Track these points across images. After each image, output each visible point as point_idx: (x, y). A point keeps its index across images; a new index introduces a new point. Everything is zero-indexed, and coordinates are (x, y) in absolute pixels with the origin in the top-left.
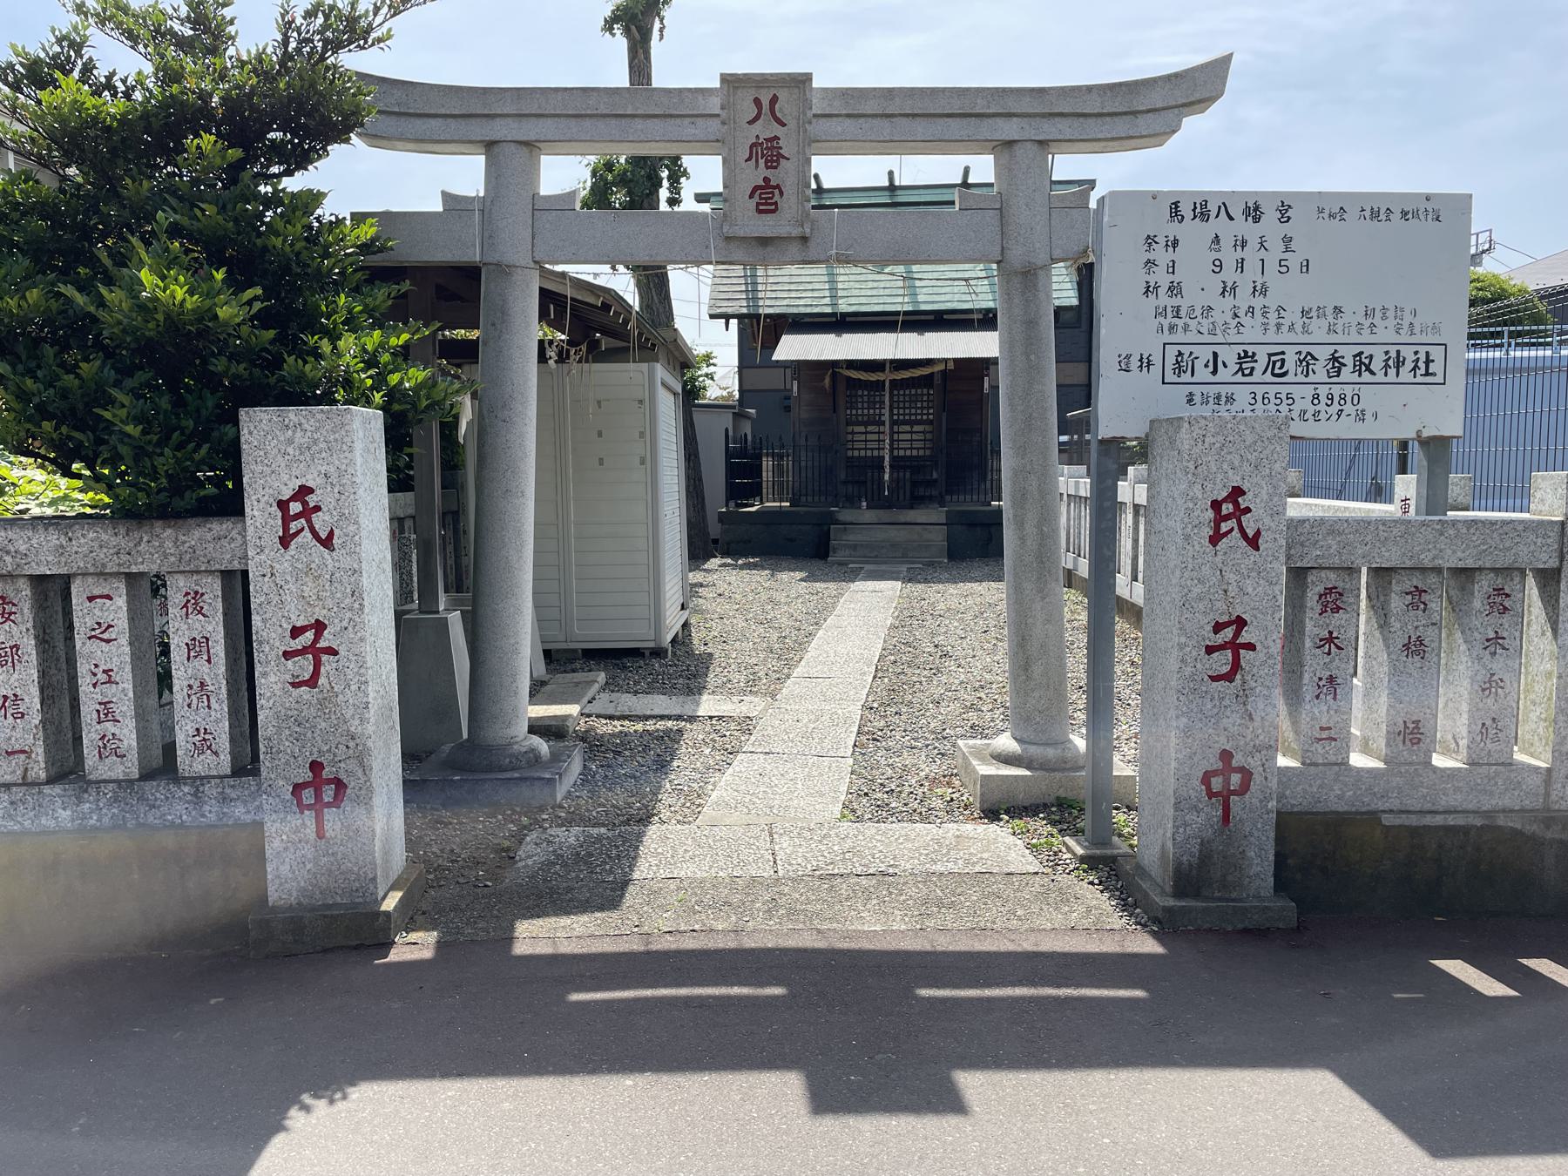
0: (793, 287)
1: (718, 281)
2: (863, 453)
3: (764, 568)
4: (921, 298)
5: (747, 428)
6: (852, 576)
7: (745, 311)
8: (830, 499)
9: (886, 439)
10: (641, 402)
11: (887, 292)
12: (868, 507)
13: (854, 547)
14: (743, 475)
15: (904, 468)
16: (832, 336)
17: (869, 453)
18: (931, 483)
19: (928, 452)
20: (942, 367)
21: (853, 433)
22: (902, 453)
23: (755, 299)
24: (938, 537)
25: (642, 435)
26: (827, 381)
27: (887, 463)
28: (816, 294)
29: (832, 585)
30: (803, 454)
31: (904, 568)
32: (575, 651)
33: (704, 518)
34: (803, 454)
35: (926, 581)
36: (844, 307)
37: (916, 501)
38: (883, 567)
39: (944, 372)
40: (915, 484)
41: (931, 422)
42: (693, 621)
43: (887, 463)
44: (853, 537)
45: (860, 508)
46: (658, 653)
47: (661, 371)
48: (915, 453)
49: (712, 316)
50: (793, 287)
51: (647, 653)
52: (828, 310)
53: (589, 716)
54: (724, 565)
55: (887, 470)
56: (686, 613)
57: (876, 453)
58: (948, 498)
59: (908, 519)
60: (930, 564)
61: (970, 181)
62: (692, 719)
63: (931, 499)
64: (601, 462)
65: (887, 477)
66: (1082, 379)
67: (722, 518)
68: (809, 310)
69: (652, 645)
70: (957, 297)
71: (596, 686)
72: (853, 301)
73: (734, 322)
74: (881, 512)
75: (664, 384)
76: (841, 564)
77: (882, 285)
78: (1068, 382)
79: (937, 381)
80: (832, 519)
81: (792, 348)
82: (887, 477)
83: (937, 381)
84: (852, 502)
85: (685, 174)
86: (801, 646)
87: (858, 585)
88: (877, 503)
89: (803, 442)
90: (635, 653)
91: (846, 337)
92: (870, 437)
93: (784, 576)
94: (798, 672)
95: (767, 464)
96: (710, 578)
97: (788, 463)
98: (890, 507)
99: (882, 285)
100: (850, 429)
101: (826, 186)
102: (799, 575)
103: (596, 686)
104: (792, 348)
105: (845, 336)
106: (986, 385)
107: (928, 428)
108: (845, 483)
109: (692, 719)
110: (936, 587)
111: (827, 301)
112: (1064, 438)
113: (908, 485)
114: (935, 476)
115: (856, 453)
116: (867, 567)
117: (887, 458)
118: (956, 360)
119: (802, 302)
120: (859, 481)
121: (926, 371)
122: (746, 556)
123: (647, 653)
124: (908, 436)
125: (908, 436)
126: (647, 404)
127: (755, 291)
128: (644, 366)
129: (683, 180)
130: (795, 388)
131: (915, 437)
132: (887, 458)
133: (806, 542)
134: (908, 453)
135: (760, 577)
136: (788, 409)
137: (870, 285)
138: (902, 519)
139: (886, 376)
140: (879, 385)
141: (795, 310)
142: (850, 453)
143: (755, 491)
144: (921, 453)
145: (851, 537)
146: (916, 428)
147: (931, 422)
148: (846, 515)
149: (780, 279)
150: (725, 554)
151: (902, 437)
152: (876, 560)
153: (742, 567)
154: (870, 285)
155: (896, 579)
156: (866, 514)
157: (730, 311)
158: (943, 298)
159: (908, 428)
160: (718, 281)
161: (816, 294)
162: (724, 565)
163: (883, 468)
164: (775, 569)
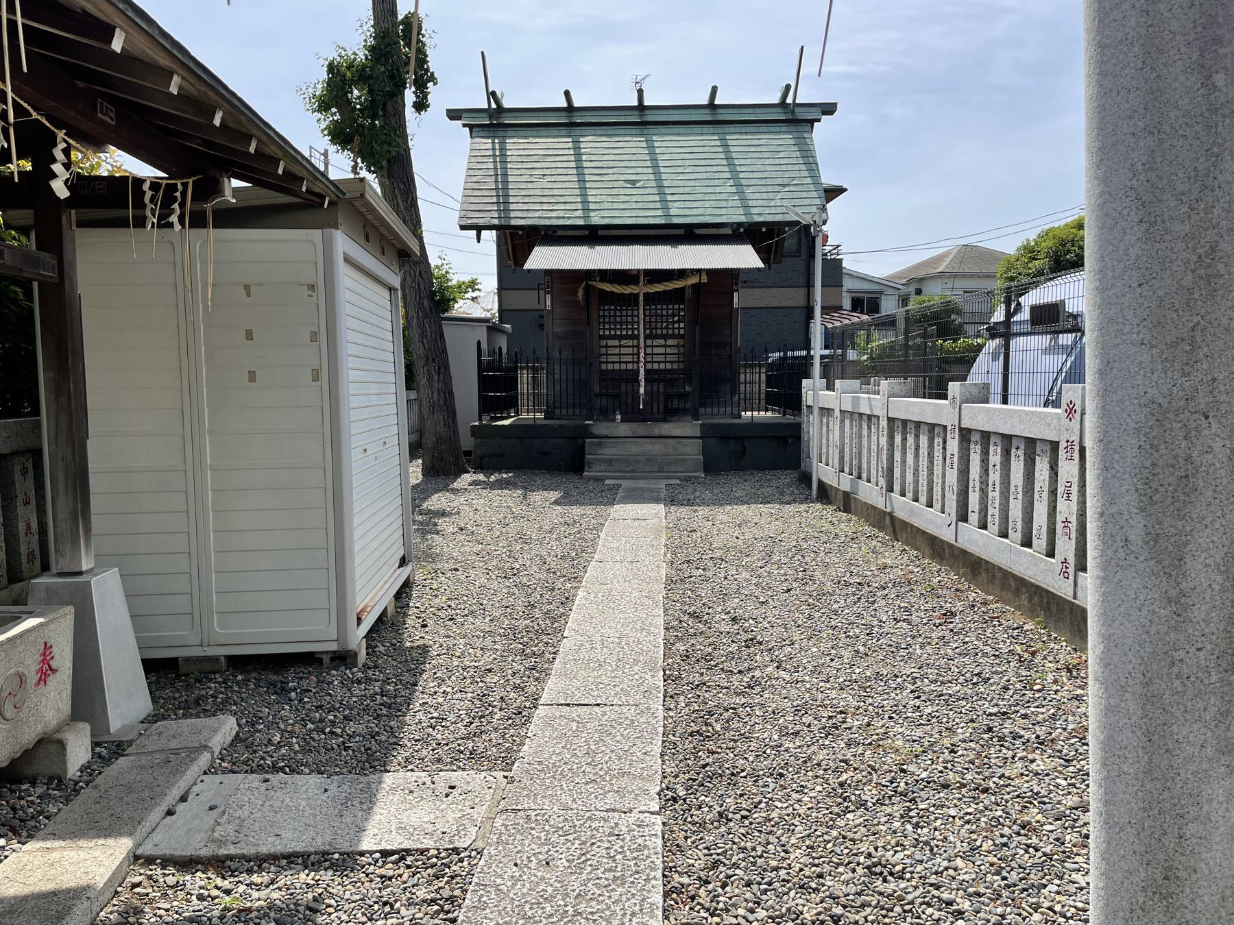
0: (545, 200)
1: (468, 192)
2: (617, 366)
3: (516, 487)
4: (673, 212)
5: (503, 343)
6: (609, 497)
7: (496, 222)
8: (584, 412)
9: (642, 352)
10: (312, 287)
11: (639, 205)
12: (622, 421)
13: (610, 462)
14: (497, 388)
15: (659, 381)
16: (585, 249)
17: (623, 366)
18: (683, 396)
19: (681, 366)
20: (694, 280)
21: (607, 346)
22: (656, 366)
23: (507, 210)
24: (693, 450)
25: (314, 336)
26: (580, 293)
27: (642, 376)
28: (568, 207)
29: (590, 510)
30: (557, 367)
31: (662, 484)
32: (214, 659)
33: (456, 431)
34: (557, 367)
35: (690, 503)
36: (596, 219)
37: (669, 414)
38: (641, 484)
39: (695, 287)
40: (668, 397)
41: (682, 337)
42: (418, 577)
43: (642, 376)
44: (608, 452)
45: (614, 420)
46: (343, 658)
47: (343, 243)
48: (669, 366)
49: (463, 228)
50: (545, 200)
51: (326, 659)
52: (581, 222)
53: (149, 860)
54: (474, 483)
55: (642, 384)
56: (407, 570)
57: (630, 366)
58: (702, 410)
59: (663, 432)
60: (687, 479)
61: (716, 102)
62: (344, 862)
63: (684, 412)
64: (252, 376)
65: (642, 390)
66: (801, 302)
67: (475, 431)
68: (561, 222)
69: (333, 647)
70: (709, 211)
71: (204, 759)
72: (606, 213)
73: (490, 236)
74: (635, 426)
75: (348, 260)
76: (596, 479)
77: (634, 198)
78: (833, 289)
79: (688, 293)
80: (587, 433)
81: (543, 258)
82: (642, 390)
83: (688, 293)
84: (606, 415)
85: (432, 78)
86: (554, 627)
87: (621, 510)
88: (633, 415)
89: (556, 355)
90: (308, 660)
91: (599, 249)
92: (623, 351)
93: (537, 497)
94: (552, 689)
95: (524, 378)
96: (458, 501)
97: (543, 376)
98: (644, 420)
99: (634, 198)
100: (604, 343)
101: (576, 104)
102: (554, 495)
103: (204, 759)
104: (543, 258)
105: (598, 248)
106: (736, 300)
107: (681, 342)
108: (599, 396)
109: (344, 862)
110: (703, 511)
111: (579, 213)
112: (827, 352)
113: (662, 398)
114: (688, 389)
115: (610, 367)
116: (626, 484)
117: (642, 371)
118: (710, 272)
119: (554, 214)
120: (614, 394)
121: (679, 284)
122: (500, 471)
123: (326, 659)
124: (662, 350)
125: (662, 350)
126: (324, 291)
127: (506, 203)
128: (316, 234)
129: (430, 85)
130: (549, 302)
131: (669, 350)
132: (642, 371)
133: (555, 457)
134: (662, 366)
135: (509, 499)
136: (542, 326)
137: (622, 198)
138: (656, 432)
139: (641, 289)
140: (632, 300)
141: (547, 222)
142: (604, 367)
143: (510, 403)
144: (675, 366)
145: (607, 451)
146: (670, 342)
147: (682, 337)
148: (601, 428)
149: (532, 192)
150: (480, 467)
151: (656, 350)
152: (633, 474)
153: (493, 486)
154: (622, 198)
155: (657, 500)
156: (619, 427)
157: (481, 222)
158: (695, 212)
159: (662, 342)
160: (468, 192)
161: (568, 207)
162: (474, 483)
163: (638, 381)
164: (528, 488)
